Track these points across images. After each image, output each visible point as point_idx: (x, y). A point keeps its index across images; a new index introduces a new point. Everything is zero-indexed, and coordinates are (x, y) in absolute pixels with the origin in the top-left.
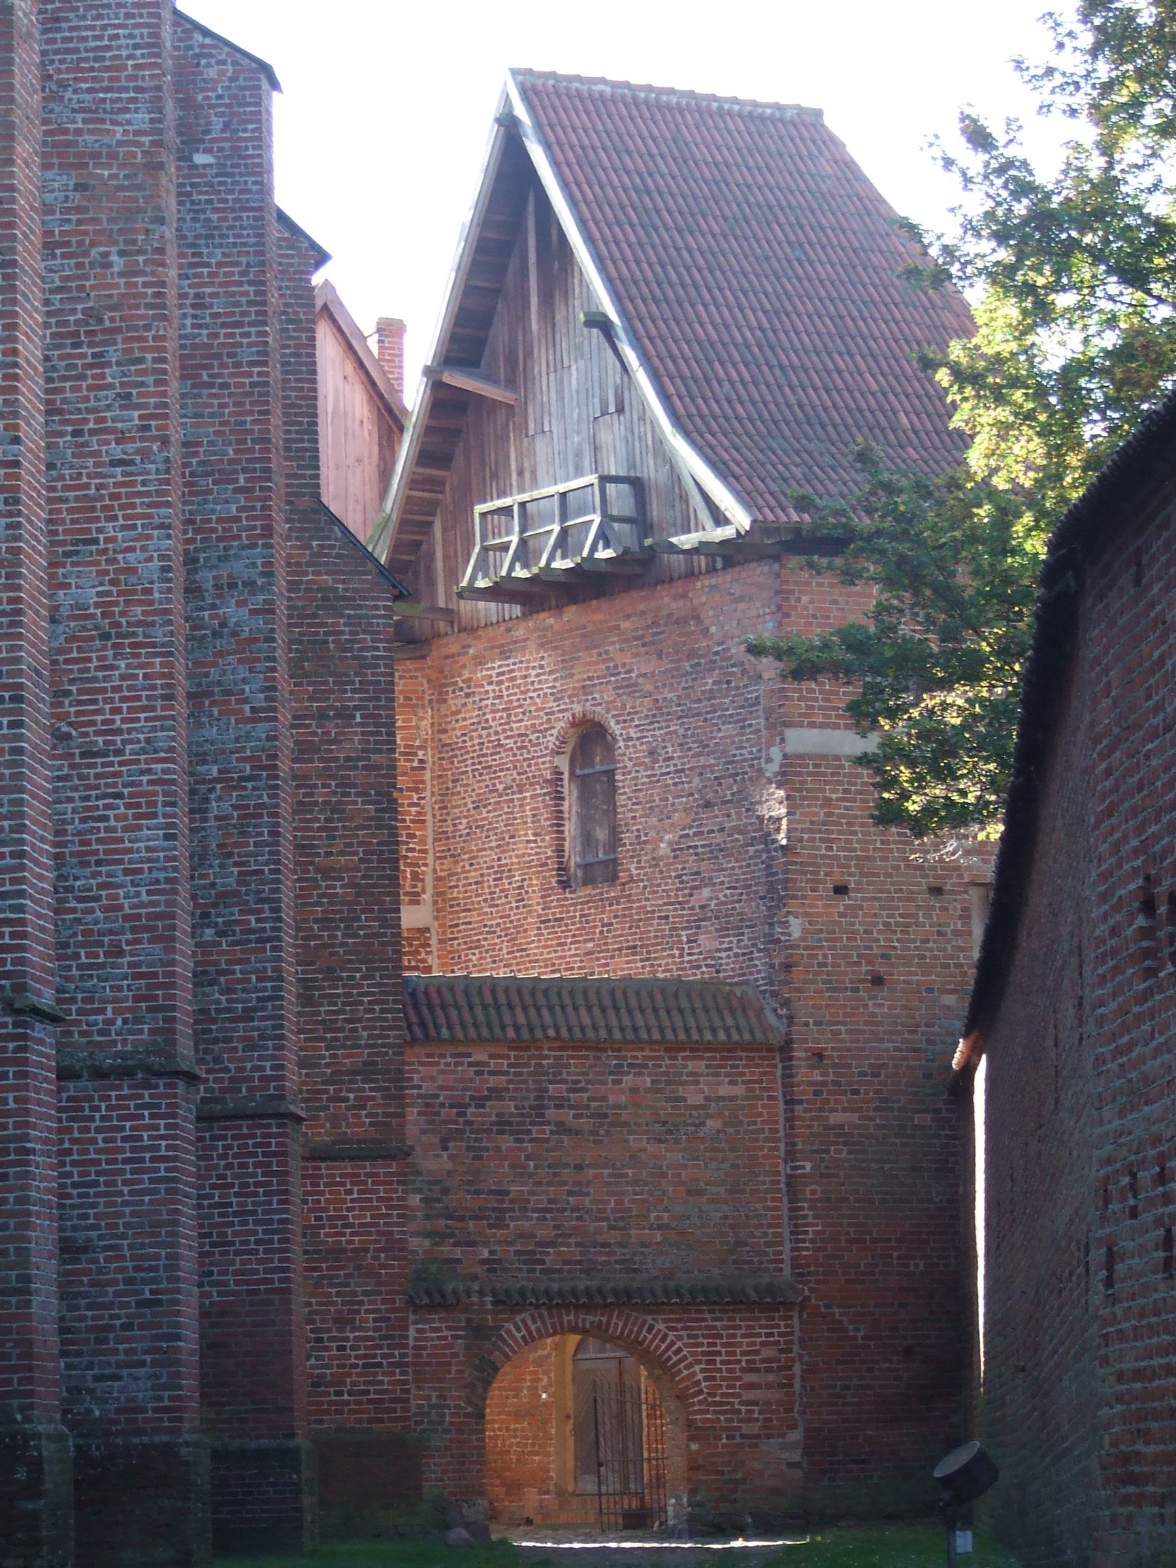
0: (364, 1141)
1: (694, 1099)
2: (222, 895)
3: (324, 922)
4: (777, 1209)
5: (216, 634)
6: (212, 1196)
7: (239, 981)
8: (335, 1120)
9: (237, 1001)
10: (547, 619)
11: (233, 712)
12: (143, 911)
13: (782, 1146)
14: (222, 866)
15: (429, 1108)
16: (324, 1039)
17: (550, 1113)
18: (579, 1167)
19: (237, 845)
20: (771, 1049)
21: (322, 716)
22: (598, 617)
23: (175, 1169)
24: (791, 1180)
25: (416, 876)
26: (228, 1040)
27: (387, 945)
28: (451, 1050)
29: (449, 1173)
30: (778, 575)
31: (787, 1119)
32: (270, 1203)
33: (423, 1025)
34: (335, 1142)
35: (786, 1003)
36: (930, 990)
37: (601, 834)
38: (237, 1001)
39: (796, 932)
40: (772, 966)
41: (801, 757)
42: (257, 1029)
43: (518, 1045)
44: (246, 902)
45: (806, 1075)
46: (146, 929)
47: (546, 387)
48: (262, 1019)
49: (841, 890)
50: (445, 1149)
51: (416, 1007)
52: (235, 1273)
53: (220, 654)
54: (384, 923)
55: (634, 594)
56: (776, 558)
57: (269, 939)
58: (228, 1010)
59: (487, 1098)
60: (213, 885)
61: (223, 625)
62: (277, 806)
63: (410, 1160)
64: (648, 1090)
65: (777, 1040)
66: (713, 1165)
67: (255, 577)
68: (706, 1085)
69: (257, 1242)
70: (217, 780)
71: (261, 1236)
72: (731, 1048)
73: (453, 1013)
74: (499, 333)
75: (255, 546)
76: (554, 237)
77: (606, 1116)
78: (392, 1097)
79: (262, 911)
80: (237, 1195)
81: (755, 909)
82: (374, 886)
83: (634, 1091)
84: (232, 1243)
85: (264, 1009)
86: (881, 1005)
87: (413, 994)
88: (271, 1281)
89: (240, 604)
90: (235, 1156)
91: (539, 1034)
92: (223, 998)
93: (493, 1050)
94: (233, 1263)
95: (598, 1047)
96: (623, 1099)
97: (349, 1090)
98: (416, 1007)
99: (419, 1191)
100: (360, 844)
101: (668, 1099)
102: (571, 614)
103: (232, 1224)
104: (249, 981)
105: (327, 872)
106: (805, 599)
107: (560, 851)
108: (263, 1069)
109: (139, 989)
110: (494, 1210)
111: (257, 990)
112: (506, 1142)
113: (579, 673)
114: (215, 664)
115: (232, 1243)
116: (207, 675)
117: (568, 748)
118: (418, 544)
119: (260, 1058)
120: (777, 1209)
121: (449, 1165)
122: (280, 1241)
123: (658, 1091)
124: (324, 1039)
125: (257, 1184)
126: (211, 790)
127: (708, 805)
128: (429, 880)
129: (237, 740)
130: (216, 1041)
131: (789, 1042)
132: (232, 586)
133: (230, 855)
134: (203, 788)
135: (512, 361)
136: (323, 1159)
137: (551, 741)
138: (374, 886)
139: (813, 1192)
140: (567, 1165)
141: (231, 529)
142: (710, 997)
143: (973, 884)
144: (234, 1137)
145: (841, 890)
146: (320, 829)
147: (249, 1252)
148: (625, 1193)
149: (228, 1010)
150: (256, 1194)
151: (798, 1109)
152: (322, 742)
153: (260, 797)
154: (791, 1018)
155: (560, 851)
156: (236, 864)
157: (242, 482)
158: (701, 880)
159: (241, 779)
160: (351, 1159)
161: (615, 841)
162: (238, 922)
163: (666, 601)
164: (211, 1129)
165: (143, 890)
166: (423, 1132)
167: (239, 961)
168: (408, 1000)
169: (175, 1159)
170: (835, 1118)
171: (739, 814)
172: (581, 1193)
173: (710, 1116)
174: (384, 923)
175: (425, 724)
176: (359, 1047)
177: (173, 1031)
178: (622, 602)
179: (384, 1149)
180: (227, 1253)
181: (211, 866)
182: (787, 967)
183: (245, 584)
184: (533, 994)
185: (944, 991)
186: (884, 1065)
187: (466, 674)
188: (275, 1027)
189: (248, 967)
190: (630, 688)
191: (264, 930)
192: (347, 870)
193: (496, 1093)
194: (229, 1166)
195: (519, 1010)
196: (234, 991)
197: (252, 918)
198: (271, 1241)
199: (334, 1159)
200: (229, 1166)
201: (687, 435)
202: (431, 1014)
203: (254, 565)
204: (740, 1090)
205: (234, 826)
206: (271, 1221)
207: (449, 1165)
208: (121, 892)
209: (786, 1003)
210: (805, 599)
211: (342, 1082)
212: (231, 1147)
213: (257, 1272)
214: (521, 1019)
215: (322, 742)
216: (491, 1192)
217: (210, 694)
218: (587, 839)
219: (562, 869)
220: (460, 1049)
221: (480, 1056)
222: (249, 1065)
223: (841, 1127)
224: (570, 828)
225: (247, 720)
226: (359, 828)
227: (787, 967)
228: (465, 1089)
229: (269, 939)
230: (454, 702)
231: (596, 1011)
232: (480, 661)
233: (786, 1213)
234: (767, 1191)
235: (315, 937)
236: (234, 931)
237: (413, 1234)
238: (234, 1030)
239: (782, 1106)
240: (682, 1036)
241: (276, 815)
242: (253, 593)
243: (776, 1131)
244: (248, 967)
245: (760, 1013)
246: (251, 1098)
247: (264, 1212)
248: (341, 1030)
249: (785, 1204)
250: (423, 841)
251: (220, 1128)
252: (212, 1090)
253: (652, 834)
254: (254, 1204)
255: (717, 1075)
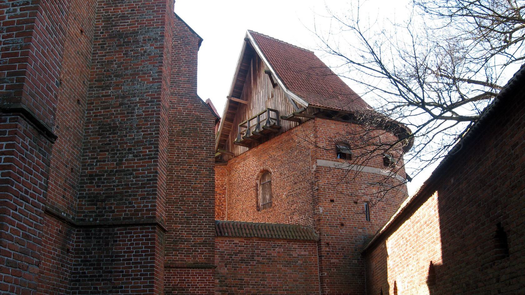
0: (202, 263)
1: (295, 255)
2: (138, 142)
3: (193, 202)
4: (317, 285)
5: (142, 55)
6: (124, 256)
7: (140, 173)
8: (195, 257)
9: (139, 181)
10: (255, 149)
11: (146, 80)
12: (16, 19)
13: (318, 268)
14: (137, 132)
15: (222, 255)
16: (192, 234)
17: (256, 258)
18: (263, 273)
19: (143, 124)
20: (315, 242)
21: (195, 147)
22: (267, 145)
23: (9, 174)
24: (321, 278)
25: (223, 214)
26: (135, 195)
27: (210, 211)
28: (228, 239)
29: (227, 274)
30: (314, 122)
31: (319, 261)
32: (147, 259)
33: (221, 232)
34: (194, 263)
35: (319, 230)
36: (355, 228)
37: (268, 197)
38: (139, 181)
39: (321, 211)
40: (314, 221)
41: (321, 167)
42: (147, 191)
43: (247, 238)
44: (146, 145)
45: (324, 249)
46: (16, 29)
47: (255, 97)
48: (148, 187)
49: (332, 201)
50: (226, 267)
51: (219, 228)
52: (132, 287)
53: (143, 61)
54: (210, 203)
55: (276, 138)
56: (313, 119)
57: (153, 158)
58: (135, 184)
59: (238, 253)
60: (134, 139)
61: (145, 52)
62: (159, 111)
63: (216, 269)
64: (282, 252)
65: (317, 239)
66: (300, 273)
67: (157, 37)
68: (298, 251)
69: (141, 275)
70: (139, 102)
71: (142, 272)
72: (305, 241)
73: (229, 230)
74: (244, 90)
75: (159, 28)
76: (257, 58)
77: (271, 259)
78: (212, 251)
79: (151, 148)
80: (134, 256)
81: (309, 207)
82: (208, 193)
83: (279, 252)
84: (131, 275)
85: (150, 184)
86: (343, 231)
87: (218, 225)
88: (146, 291)
89: (151, 45)
90: (134, 240)
91: (253, 236)
92: (134, 180)
93: (240, 240)
94: (131, 283)
95: (269, 239)
96: (276, 255)
97: (199, 249)
98: (219, 228)
99: (219, 279)
100: (204, 181)
101: (288, 255)
102: (260, 147)
103: (132, 267)
104: (144, 173)
105: (195, 188)
106: (321, 129)
107: (257, 202)
108: (148, 206)
109: (6, 63)
110: (240, 284)
111: (147, 177)
112: (244, 266)
113: (262, 160)
114: (141, 65)
115: (131, 275)
116: (138, 68)
117: (259, 178)
118: (226, 140)
119: (147, 202)
120: (317, 285)
121: (227, 272)
122: (150, 274)
123: (286, 253)
124: (192, 234)
125: (142, 252)
126: (135, 106)
127: (296, 183)
128: (226, 214)
129: (146, 89)
130: (130, 196)
131: (320, 240)
132: (149, 40)
133: (141, 128)
134: (132, 105)
135: (247, 96)
136: (190, 268)
137: (255, 177)
138: (208, 193)
139: (327, 281)
140: (260, 273)
141: (150, 23)
142: (296, 228)
143: (364, 201)
144: (135, 233)
145: (332, 201)
146: (193, 177)
147: (138, 279)
148: (276, 281)
149: (135, 184)
150: (142, 255)
151: (323, 258)
152: (195, 154)
153: (154, 108)
154: (320, 234)
155: (257, 202)
156: (143, 131)
157: (156, 9)
158: (293, 202)
159: (147, 102)
160: (199, 268)
161: (271, 196)
162: (141, 152)
163: (284, 137)
164: (126, 229)
165: (18, 9)
166: (220, 262)
167: (141, 166)
168: (217, 226)
169: (9, 167)
170: (332, 261)
171: (304, 184)
172: (264, 280)
173: (299, 260)
174: (210, 203)
175: (226, 180)
176: (202, 236)
177: (21, 86)
178: (273, 141)
179: (208, 266)
180: (129, 279)
181: (133, 132)
182: (319, 220)
183: (153, 39)
184: (251, 226)
185: (358, 228)
186: (345, 247)
187: (236, 167)
188: (153, 191)
189: (144, 168)
190: (275, 160)
191: (151, 155)
192: (201, 188)
193: (241, 252)
194: (132, 244)
195: (247, 230)
196: (139, 177)
197: (147, 150)
198: (147, 275)
199: (193, 268)
200: (132, 244)
201: (291, 91)
202: (220, 230)
203: (157, 33)
204: (307, 253)
205: (143, 118)
206: (147, 267)
207: (227, 272)
208: (5, 10)
209: (319, 230)
210: (321, 129)
211: (197, 246)
212: (133, 237)
213: (140, 287)
214: (248, 232)
215: (195, 154)
216: (239, 279)
217: (138, 74)
218: (264, 198)
219: (258, 206)
220: (231, 239)
221: (236, 241)
222: (142, 205)
223: (334, 263)
224: (260, 197)
225: (152, 82)
226: (204, 177)
227: (319, 220)
228: (232, 250)
229: (153, 158)
230: (232, 174)
231: (268, 231)
232: (239, 163)
233: (320, 287)
234: (315, 281)
235: (190, 206)
236: (140, 155)
237: (217, 291)
238: (137, 192)
239: (318, 257)
240: (291, 238)
241: (159, 114)
242: (156, 42)
243: (316, 264)
244: (144, 168)
245: (311, 233)
246: (143, 217)
247: (144, 263)
248: (197, 232)
249: (319, 285)
250: (225, 206)
251: (129, 229)
252: (127, 215)
253: (281, 193)
254: (141, 259)
255: (301, 249)
